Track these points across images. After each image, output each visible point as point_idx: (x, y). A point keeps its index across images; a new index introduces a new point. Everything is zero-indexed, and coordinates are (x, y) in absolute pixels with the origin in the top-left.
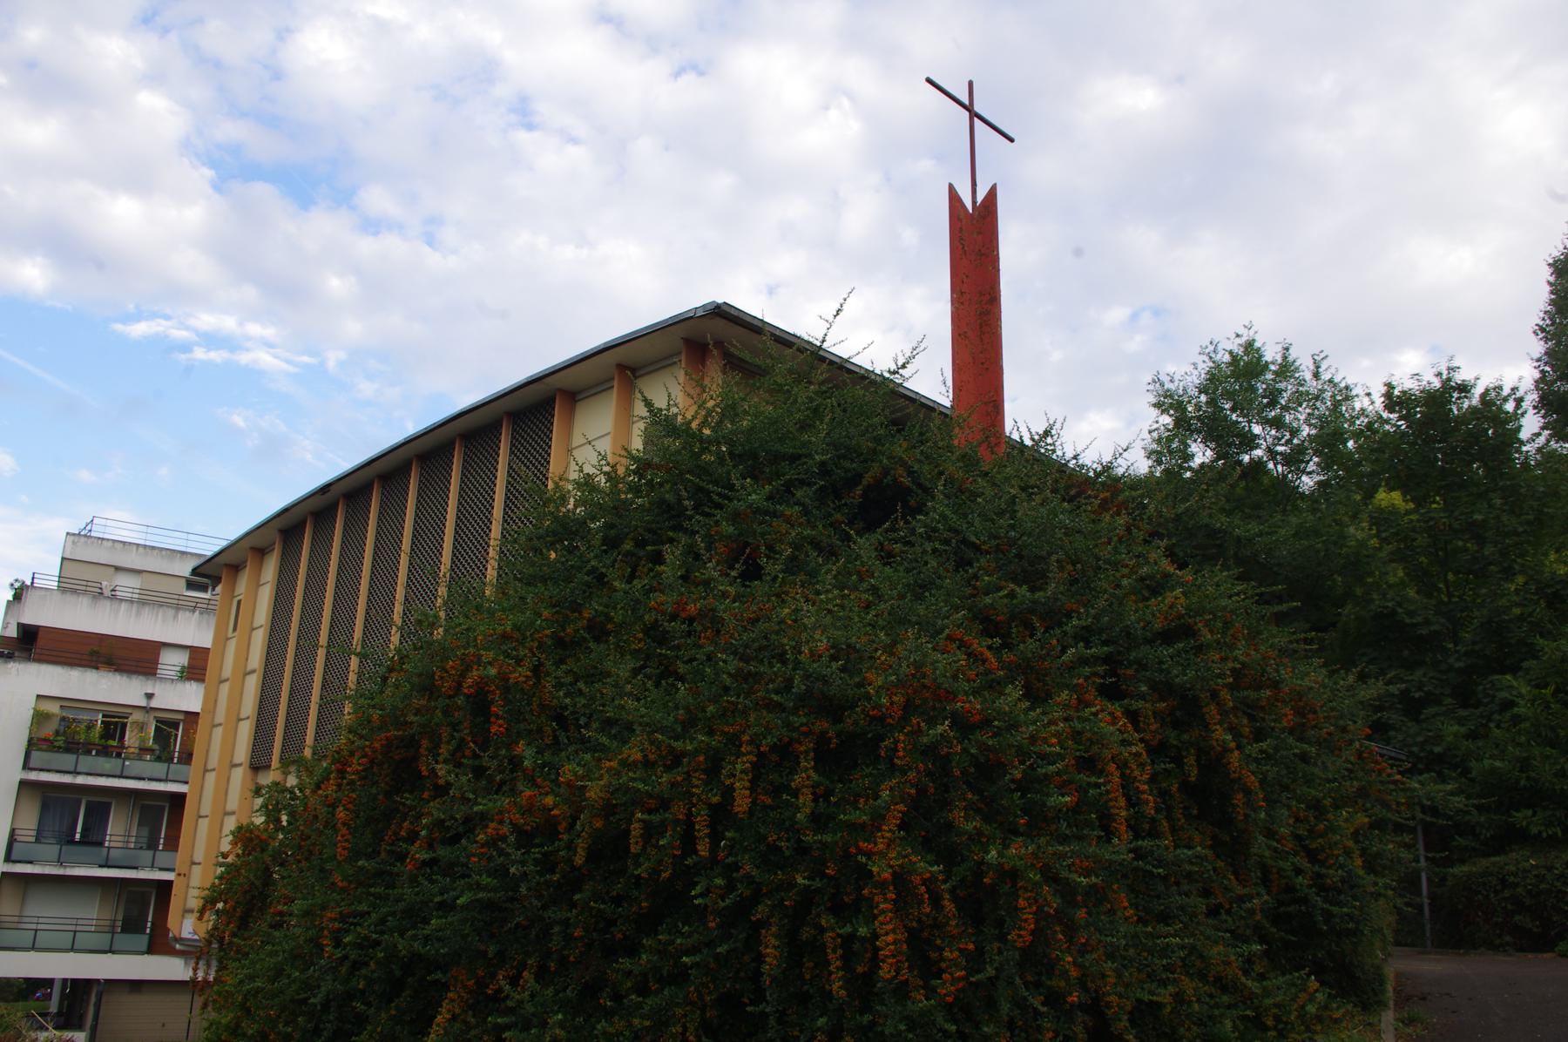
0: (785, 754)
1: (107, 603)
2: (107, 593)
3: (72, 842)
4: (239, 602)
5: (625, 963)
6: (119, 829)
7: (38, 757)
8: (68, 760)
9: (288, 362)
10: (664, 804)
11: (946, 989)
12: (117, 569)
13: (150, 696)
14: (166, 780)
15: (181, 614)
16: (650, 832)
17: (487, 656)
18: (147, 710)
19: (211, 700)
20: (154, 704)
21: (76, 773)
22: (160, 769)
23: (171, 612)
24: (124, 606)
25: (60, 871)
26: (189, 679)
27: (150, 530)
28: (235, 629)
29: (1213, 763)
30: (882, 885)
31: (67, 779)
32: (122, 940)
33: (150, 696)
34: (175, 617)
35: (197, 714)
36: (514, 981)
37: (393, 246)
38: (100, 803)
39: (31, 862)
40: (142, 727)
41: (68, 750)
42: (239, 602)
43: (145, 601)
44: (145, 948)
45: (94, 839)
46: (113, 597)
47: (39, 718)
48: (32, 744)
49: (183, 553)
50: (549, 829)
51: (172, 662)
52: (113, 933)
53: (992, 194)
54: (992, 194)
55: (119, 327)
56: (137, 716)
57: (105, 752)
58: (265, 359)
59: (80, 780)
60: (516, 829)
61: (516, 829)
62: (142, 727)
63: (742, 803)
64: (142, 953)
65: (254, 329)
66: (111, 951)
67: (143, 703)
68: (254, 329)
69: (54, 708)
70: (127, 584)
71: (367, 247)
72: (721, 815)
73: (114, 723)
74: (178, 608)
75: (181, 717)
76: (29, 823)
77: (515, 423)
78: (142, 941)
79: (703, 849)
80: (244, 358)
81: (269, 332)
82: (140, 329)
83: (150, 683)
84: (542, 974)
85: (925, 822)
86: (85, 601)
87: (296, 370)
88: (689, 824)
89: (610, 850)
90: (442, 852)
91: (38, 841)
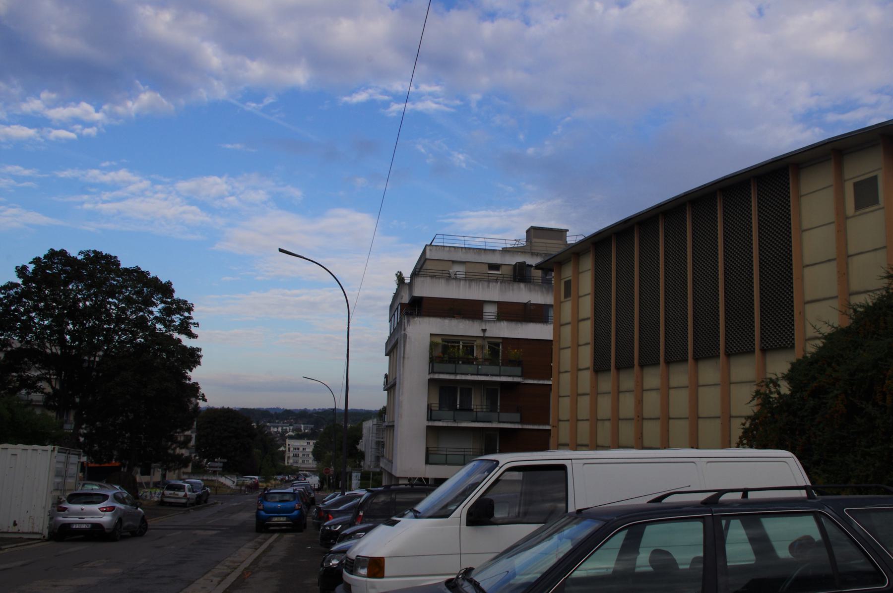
1: (454, 282)
2: (453, 276)
3: (457, 410)
6: (477, 402)
7: (437, 367)
8: (451, 367)
9: (446, 105)
12: (454, 262)
13: (484, 331)
15: (491, 284)
18: (484, 338)
19: (557, 332)
20: (487, 335)
21: (455, 373)
22: (495, 369)
23: (486, 284)
24: (462, 282)
25: (455, 425)
26: (502, 320)
31: (452, 377)
33: (484, 331)
34: (488, 286)
35: (551, 341)
37: (505, 27)
38: (468, 388)
39: (440, 420)
40: (482, 347)
41: (450, 362)
43: (470, 279)
45: (466, 408)
46: (456, 279)
47: (433, 345)
48: (432, 360)
49: (485, 250)
51: (490, 311)
55: (346, 99)
56: (479, 342)
57: (468, 362)
58: (429, 106)
59: (459, 377)
62: (482, 347)
65: (425, 88)
67: (482, 335)
68: (425, 88)
69: (439, 340)
70: (459, 270)
71: (488, 29)
73: (469, 344)
74: (489, 281)
76: (436, 401)
80: (420, 106)
81: (436, 89)
82: (361, 97)
83: (483, 324)
86: (443, 282)
87: (453, 110)
91: (440, 409)
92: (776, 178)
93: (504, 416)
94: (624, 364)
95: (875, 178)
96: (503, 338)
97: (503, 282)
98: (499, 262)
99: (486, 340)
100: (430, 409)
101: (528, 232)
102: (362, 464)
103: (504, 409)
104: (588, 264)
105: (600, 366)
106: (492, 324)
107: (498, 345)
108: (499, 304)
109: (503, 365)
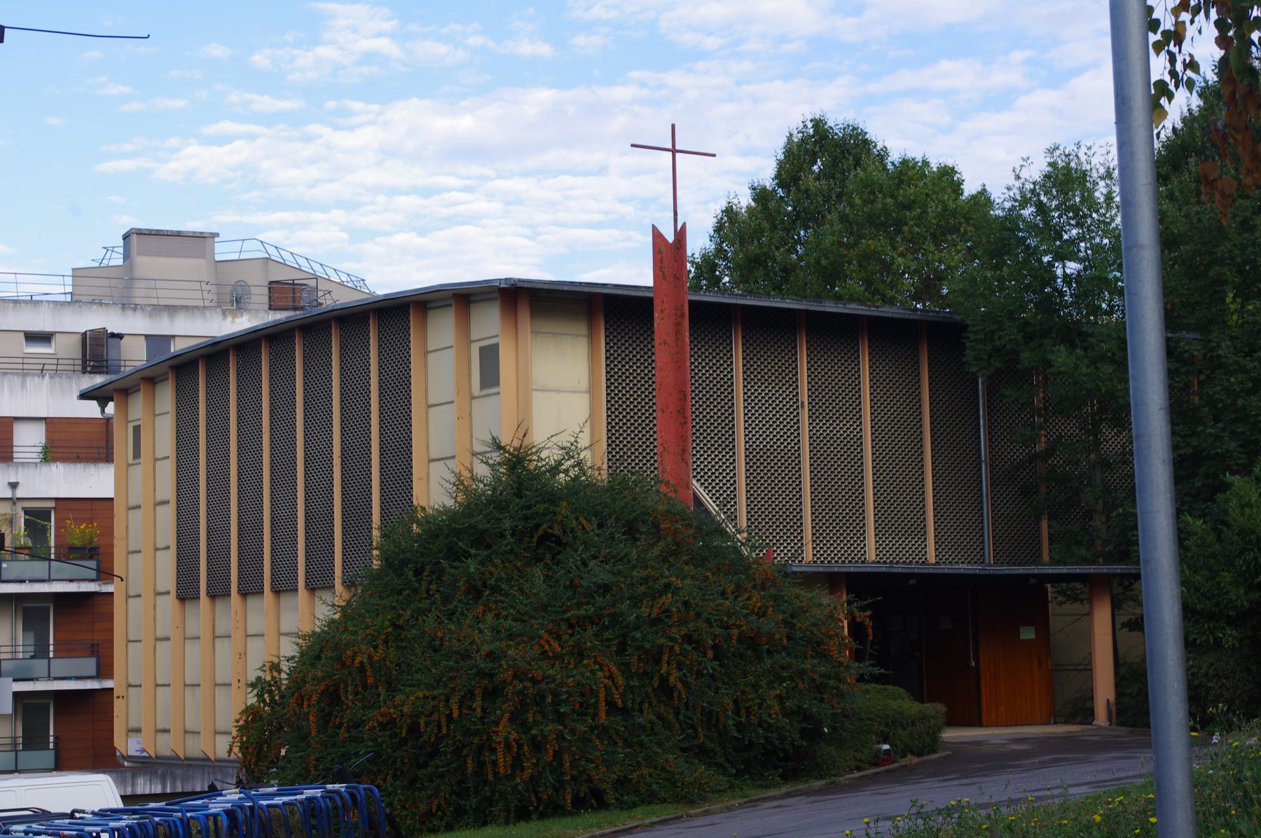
0: (471, 694)
4: (137, 430)
5: (424, 771)
10: (431, 714)
11: (526, 775)
13: (14, 486)
14: (49, 580)
15: (28, 380)
16: (427, 724)
17: (363, 647)
18: (13, 501)
20: (20, 493)
22: (39, 568)
23: (17, 380)
27: (26, 361)
28: (137, 454)
29: (664, 680)
30: (499, 743)
32: (27, 757)
33: (14, 486)
34: (23, 385)
36: (384, 781)
42: (137, 430)
44: (52, 765)
50: (392, 722)
52: (16, 751)
53: (684, 225)
54: (684, 225)
60: (380, 724)
61: (380, 724)
63: (456, 714)
64: (50, 770)
66: (16, 770)
67: (8, 494)
72: (449, 717)
74: (24, 373)
75: (52, 504)
77: (379, 318)
78: (48, 757)
79: (444, 731)
84: (395, 777)
85: (516, 718)
88: (439, 722)
89: (414, 729)
90: (354, 733)
92: (398, 314)
93: (59, 666)
94: (218, 592)
95: (497, 345)
96: (57, 499)
97: (56, 373)
98: (48, 328)
99: (20, 505)
100: (345, 343)
101: (126, 237)
102: (252, 700)
103: (65, 650)
104: (166, 397)
105: (186, 593)
106: (31, 471)
107: (45, 514)
108: (51, 424)
109: (57, 559)
